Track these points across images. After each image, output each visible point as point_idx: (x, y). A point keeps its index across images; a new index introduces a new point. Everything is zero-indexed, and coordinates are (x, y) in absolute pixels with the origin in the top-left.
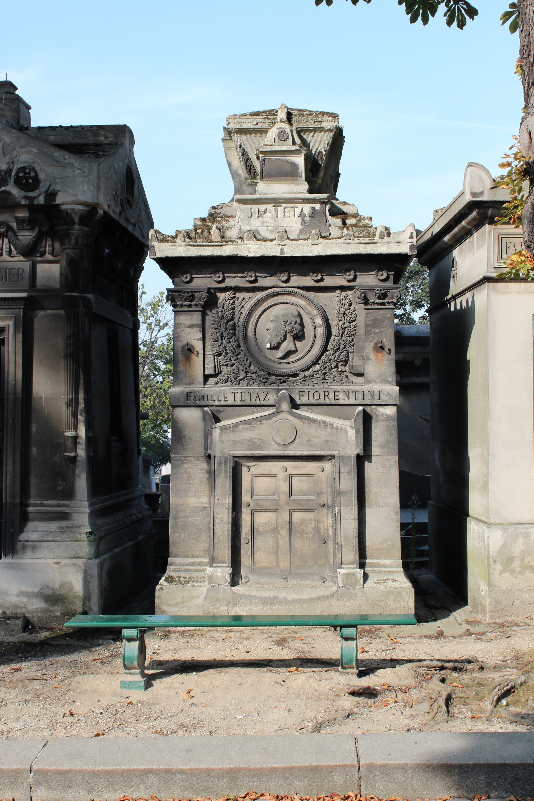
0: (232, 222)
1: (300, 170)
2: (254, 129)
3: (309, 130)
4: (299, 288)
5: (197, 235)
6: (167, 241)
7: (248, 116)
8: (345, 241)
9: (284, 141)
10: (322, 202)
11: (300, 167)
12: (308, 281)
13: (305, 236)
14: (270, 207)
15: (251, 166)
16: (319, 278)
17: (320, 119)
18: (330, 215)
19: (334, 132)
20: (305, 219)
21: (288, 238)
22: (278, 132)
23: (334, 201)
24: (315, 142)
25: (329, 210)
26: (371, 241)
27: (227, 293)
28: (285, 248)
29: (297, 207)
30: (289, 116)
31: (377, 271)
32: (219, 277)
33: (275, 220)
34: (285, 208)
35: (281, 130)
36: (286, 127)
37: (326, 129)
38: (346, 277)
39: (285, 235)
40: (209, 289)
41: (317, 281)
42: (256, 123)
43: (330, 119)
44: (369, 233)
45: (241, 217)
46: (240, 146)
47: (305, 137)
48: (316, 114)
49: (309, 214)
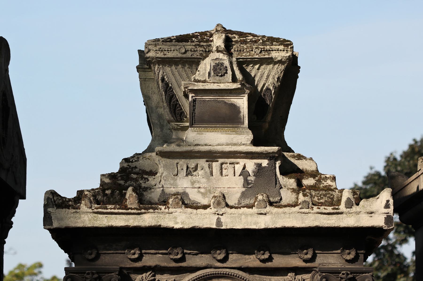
0: (152, 181)
1: (242, 114)
2: (181, 58)
3: (254, 62)
4: (240, 269)
5: (105, 198)
6: (68, 207)
7: (173, 43)
8: (301, 210)
9: (221, 76)
10: (270, 157)
11: (242, 110)
12: (252, 260)
13: (248, 201)
14: (202, 163)
15: (176, 105)
16: (266, 256)
17: (268, 47)
18: (281, 174)
19: (286, 65)
20: (249, 178)
21: (227, 205)
22: (213, 64)
23: (285, 154)
24: (262, 76)
25: (280, 167)
26: (335, 211)
27: (144, 275)
28: (223, 219)
29: (238, 163)
30: (228, 42)
31: (343, 249)
32: (134, 254)
33: (208, 179)
34: (222, 164)
35: (217, 62)
36: (224, 58)
37: (276, 60)
38: (302, 256)
39: (222, 201)
40: (121, 269)
41: (264, 261)
42: (183, 51)
43: (281, 47)
44: (332, 199)
45: (164, 175)
46: (163, 80)
47: (248, 70)
48: (263, 41)
49: (253, 172)
